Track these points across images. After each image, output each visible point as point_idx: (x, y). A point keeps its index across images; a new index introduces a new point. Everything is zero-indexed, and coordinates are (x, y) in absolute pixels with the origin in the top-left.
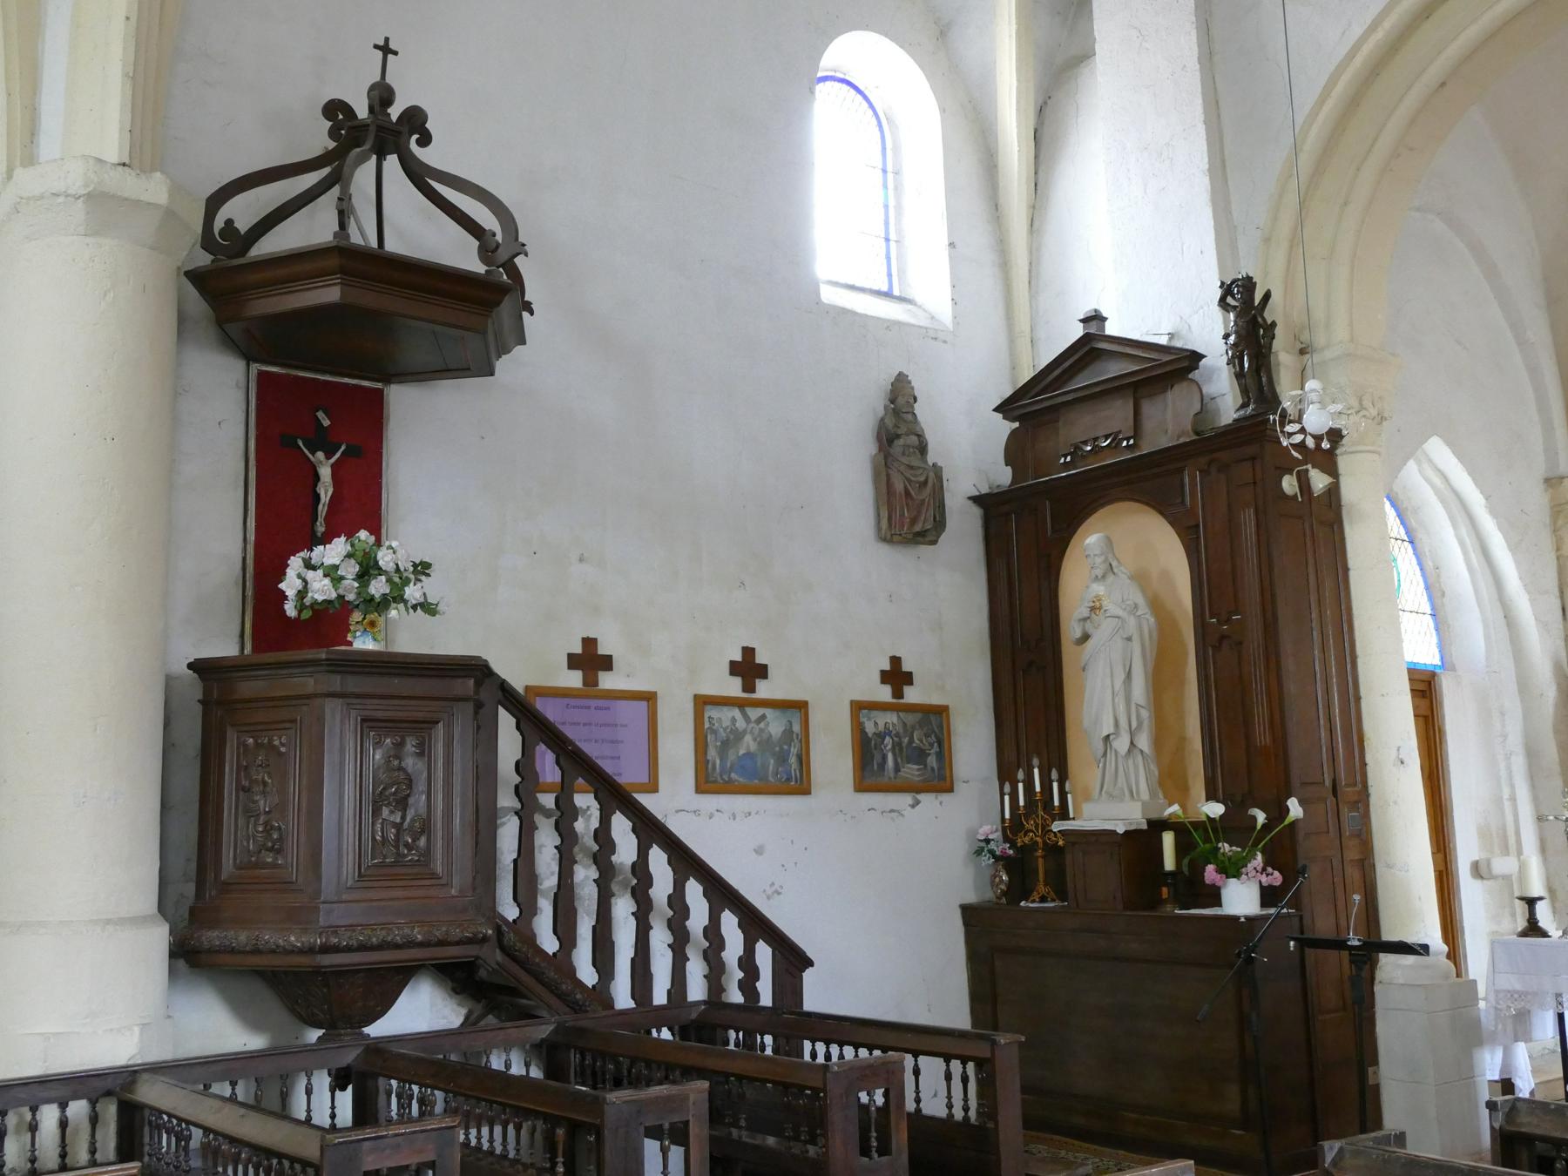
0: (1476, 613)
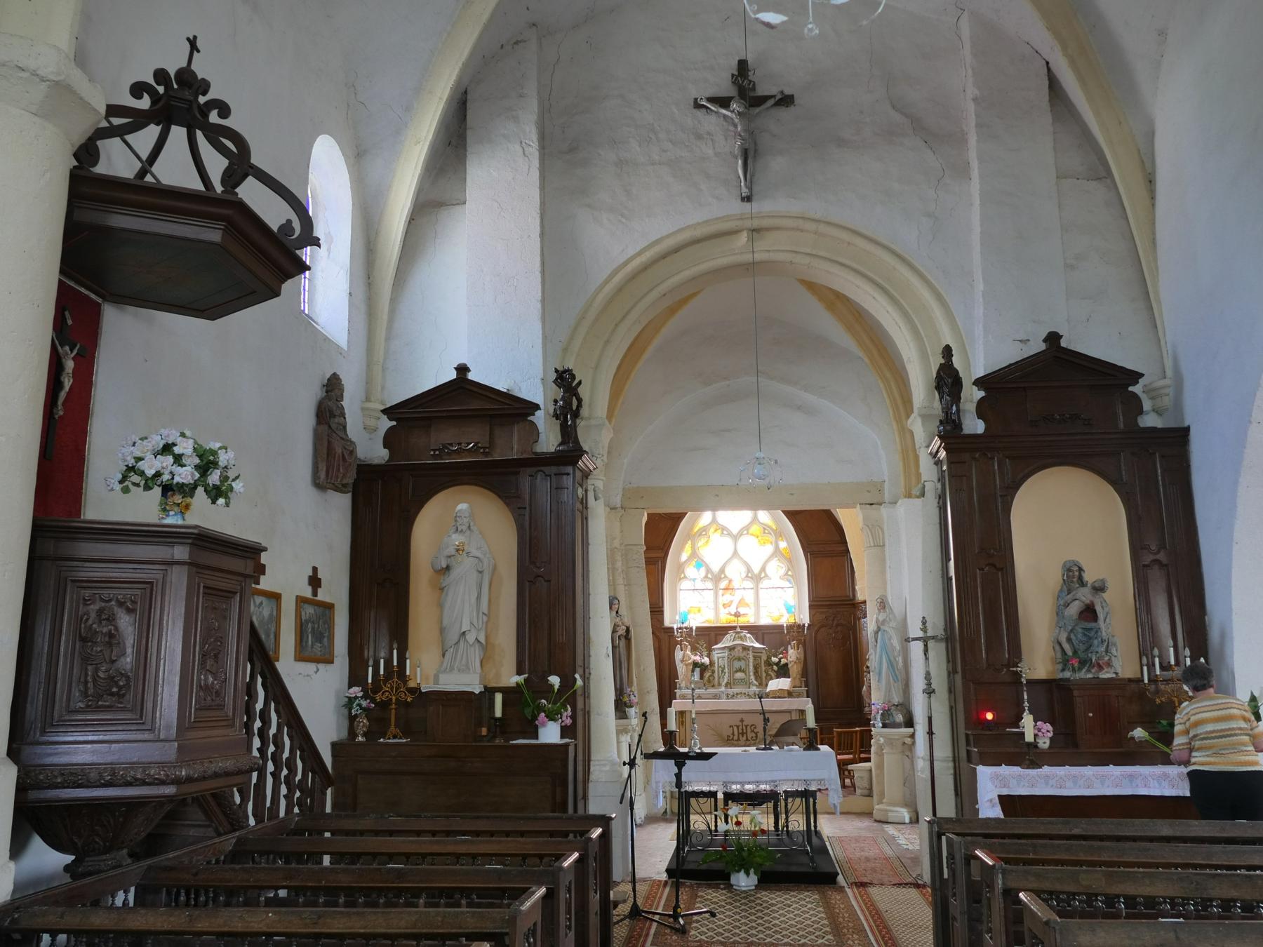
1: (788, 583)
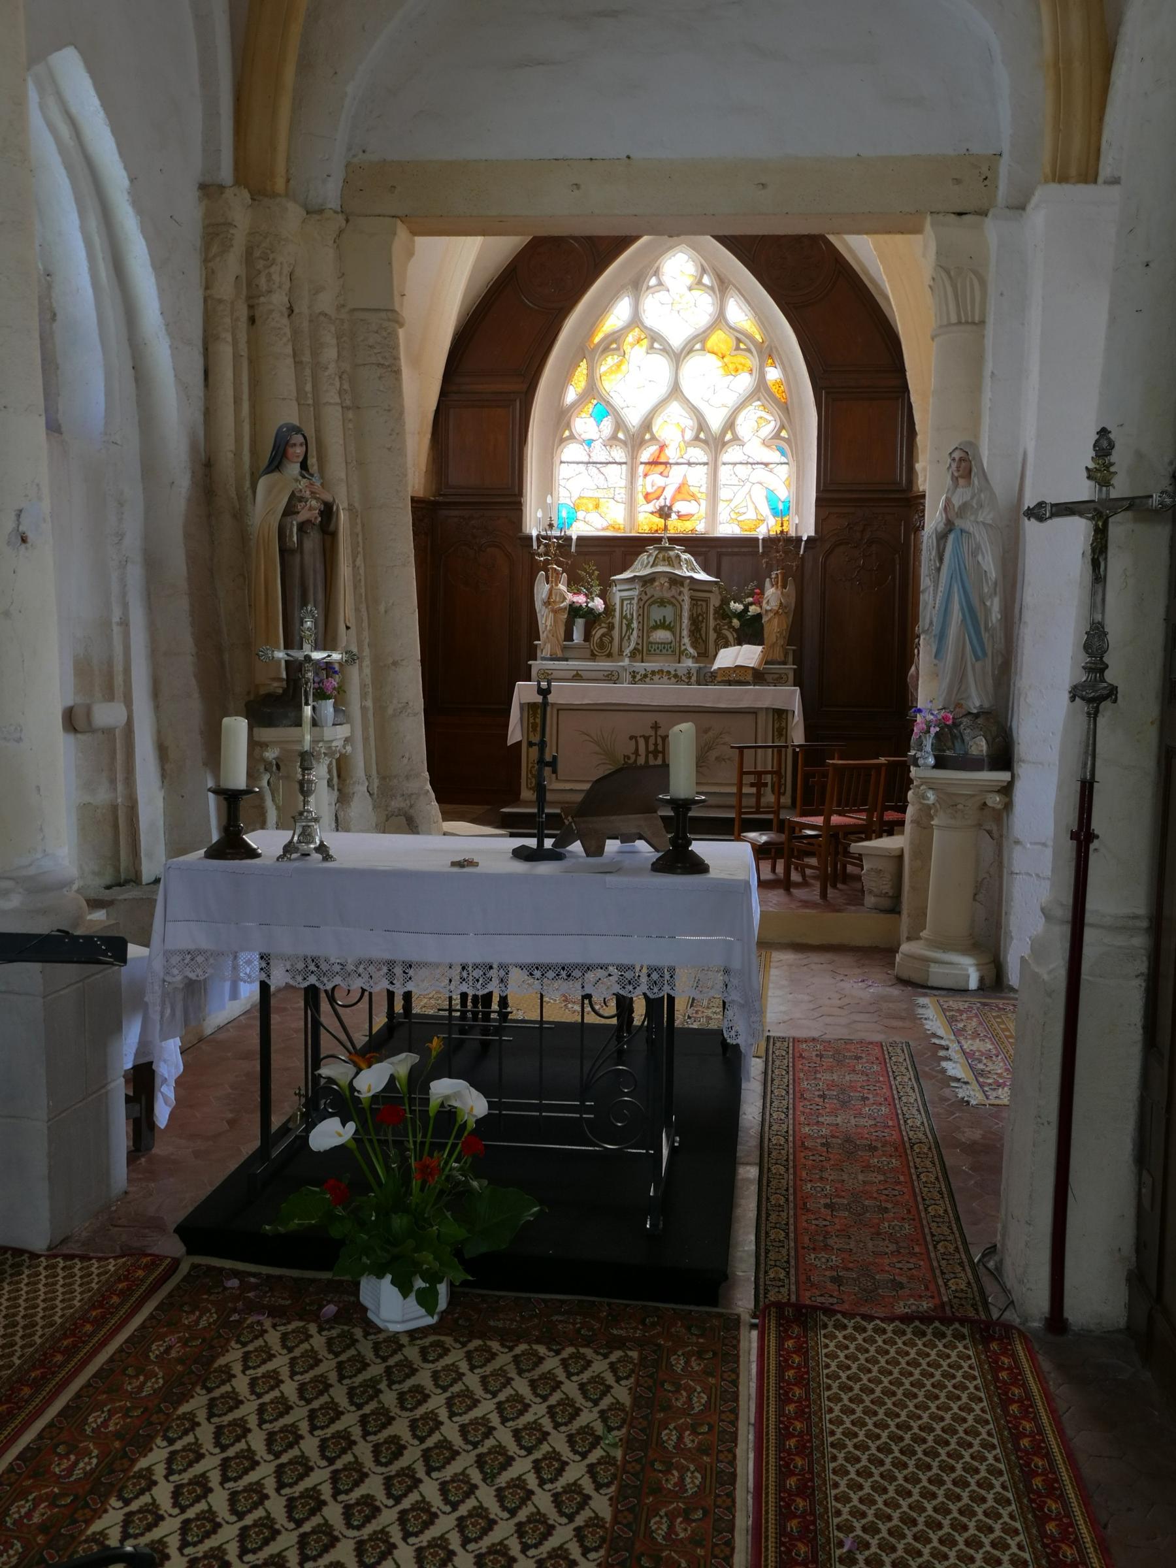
0: (98, 354)
1: (778, 453)
